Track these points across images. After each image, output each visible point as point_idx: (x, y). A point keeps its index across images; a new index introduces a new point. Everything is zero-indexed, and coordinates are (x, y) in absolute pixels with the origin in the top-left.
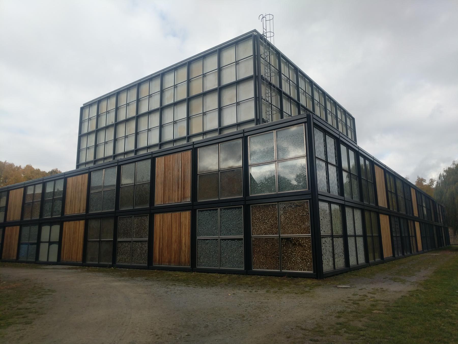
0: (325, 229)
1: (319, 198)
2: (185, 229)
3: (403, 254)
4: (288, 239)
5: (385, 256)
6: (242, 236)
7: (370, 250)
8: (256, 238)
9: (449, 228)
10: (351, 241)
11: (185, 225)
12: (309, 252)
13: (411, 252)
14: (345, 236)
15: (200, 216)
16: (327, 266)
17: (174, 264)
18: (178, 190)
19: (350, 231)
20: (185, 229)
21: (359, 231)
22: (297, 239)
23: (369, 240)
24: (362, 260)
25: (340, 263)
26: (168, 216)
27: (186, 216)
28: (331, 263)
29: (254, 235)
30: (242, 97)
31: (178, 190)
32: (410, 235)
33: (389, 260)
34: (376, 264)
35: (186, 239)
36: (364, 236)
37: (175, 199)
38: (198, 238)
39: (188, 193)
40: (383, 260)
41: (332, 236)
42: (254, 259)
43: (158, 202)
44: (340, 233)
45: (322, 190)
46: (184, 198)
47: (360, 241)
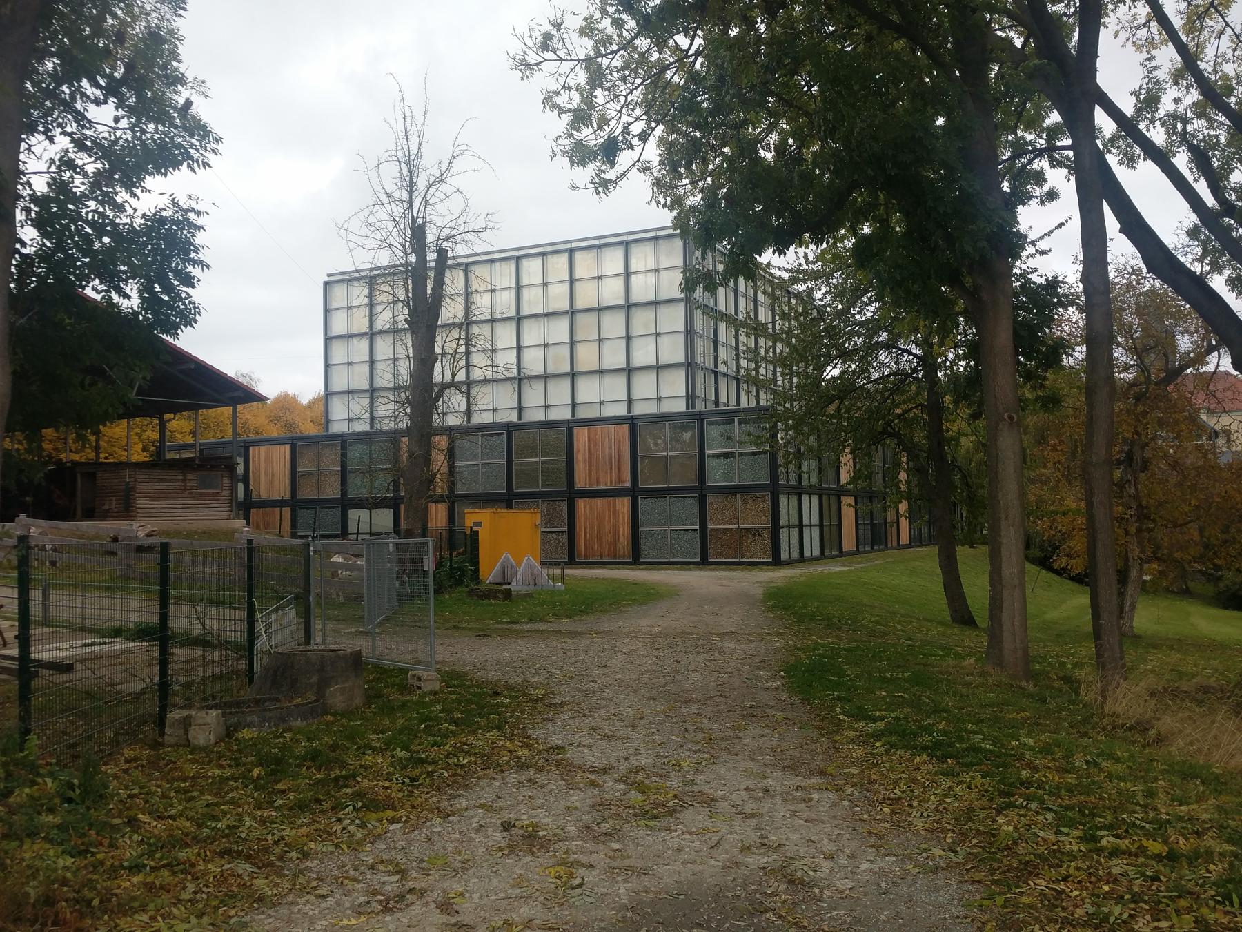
0: (783, 520)
1: (1084, 600)
2: (623, 518)
3: (872, 548)
4: (747, 529)
5: (845, 549)
6: (697, 527)
7: (826, 543)
8: (713, 529)
9: (1224, 460)
10: (806, 532)
11: (623, 513)
12: (768, 542)
13: (886, 546)
14: (801, 526)
15: (643, 505)
16: (784, 556)
17: (456, 563)
18: (611, 472)
19: (806, 521)
20: (623, 518)
21: (816, 520)
22: (757, 529)
23: (826, 529)
24: (816, 553)
25: (795, 554)
26: (598, 503)
27: (624, 504)
28: (787, 553)
29: (710, 526)
30: (665, 263)
31: (611, 472)
32: (366, 433)
33: (849, 554)
34: (832, 557)
35: (625, 530)
36: (821, 526)
37: (607, 482)
38: (641, 528)
39: (627, 475)
40: (842, 554)
41: (811, 526)
42: (711, 548)
43: (580, 483)
44: (797, 523)
45: (385, 243)
46: (620, 481)
47: (816, 531)
